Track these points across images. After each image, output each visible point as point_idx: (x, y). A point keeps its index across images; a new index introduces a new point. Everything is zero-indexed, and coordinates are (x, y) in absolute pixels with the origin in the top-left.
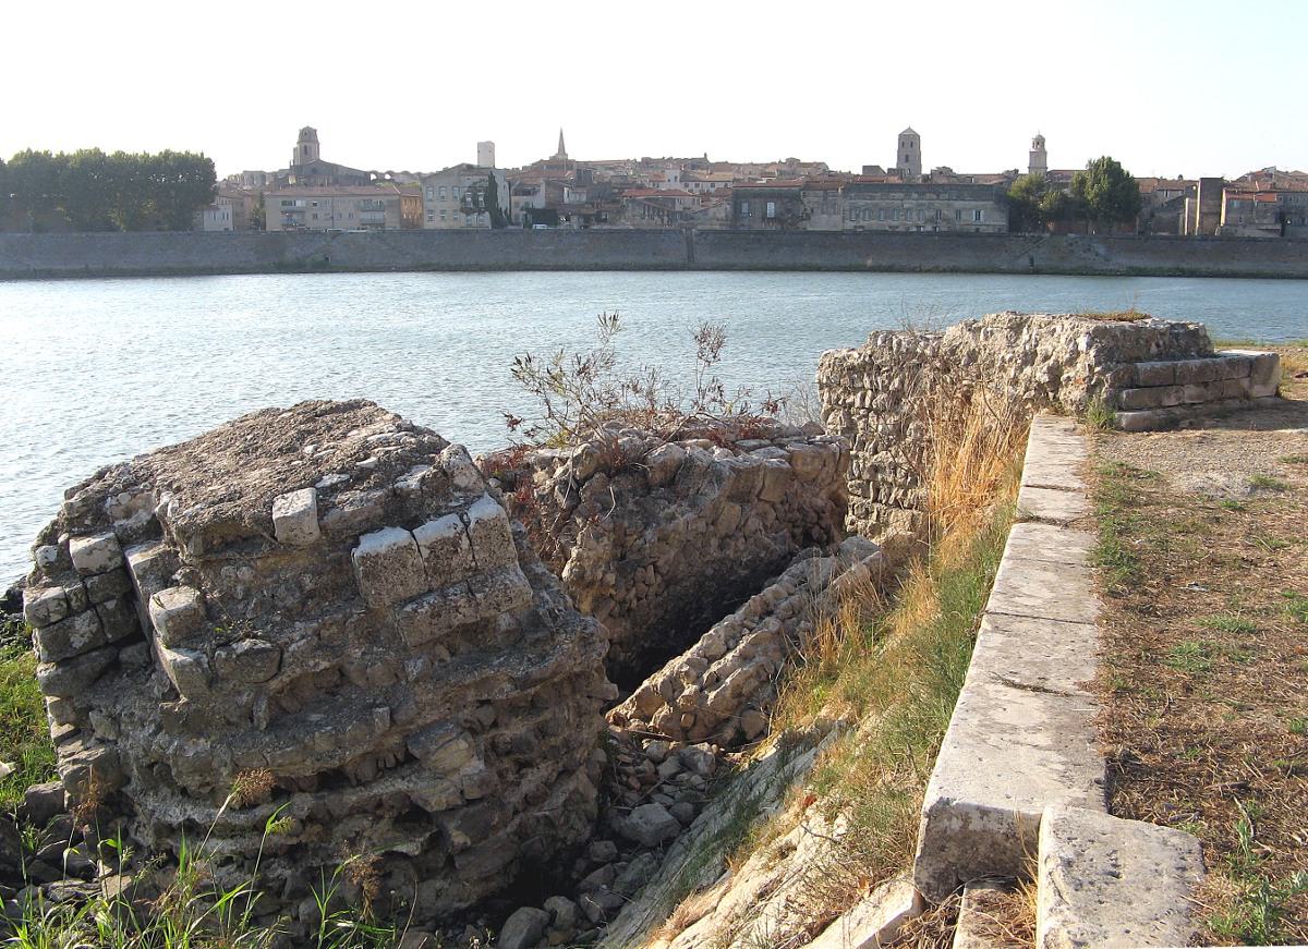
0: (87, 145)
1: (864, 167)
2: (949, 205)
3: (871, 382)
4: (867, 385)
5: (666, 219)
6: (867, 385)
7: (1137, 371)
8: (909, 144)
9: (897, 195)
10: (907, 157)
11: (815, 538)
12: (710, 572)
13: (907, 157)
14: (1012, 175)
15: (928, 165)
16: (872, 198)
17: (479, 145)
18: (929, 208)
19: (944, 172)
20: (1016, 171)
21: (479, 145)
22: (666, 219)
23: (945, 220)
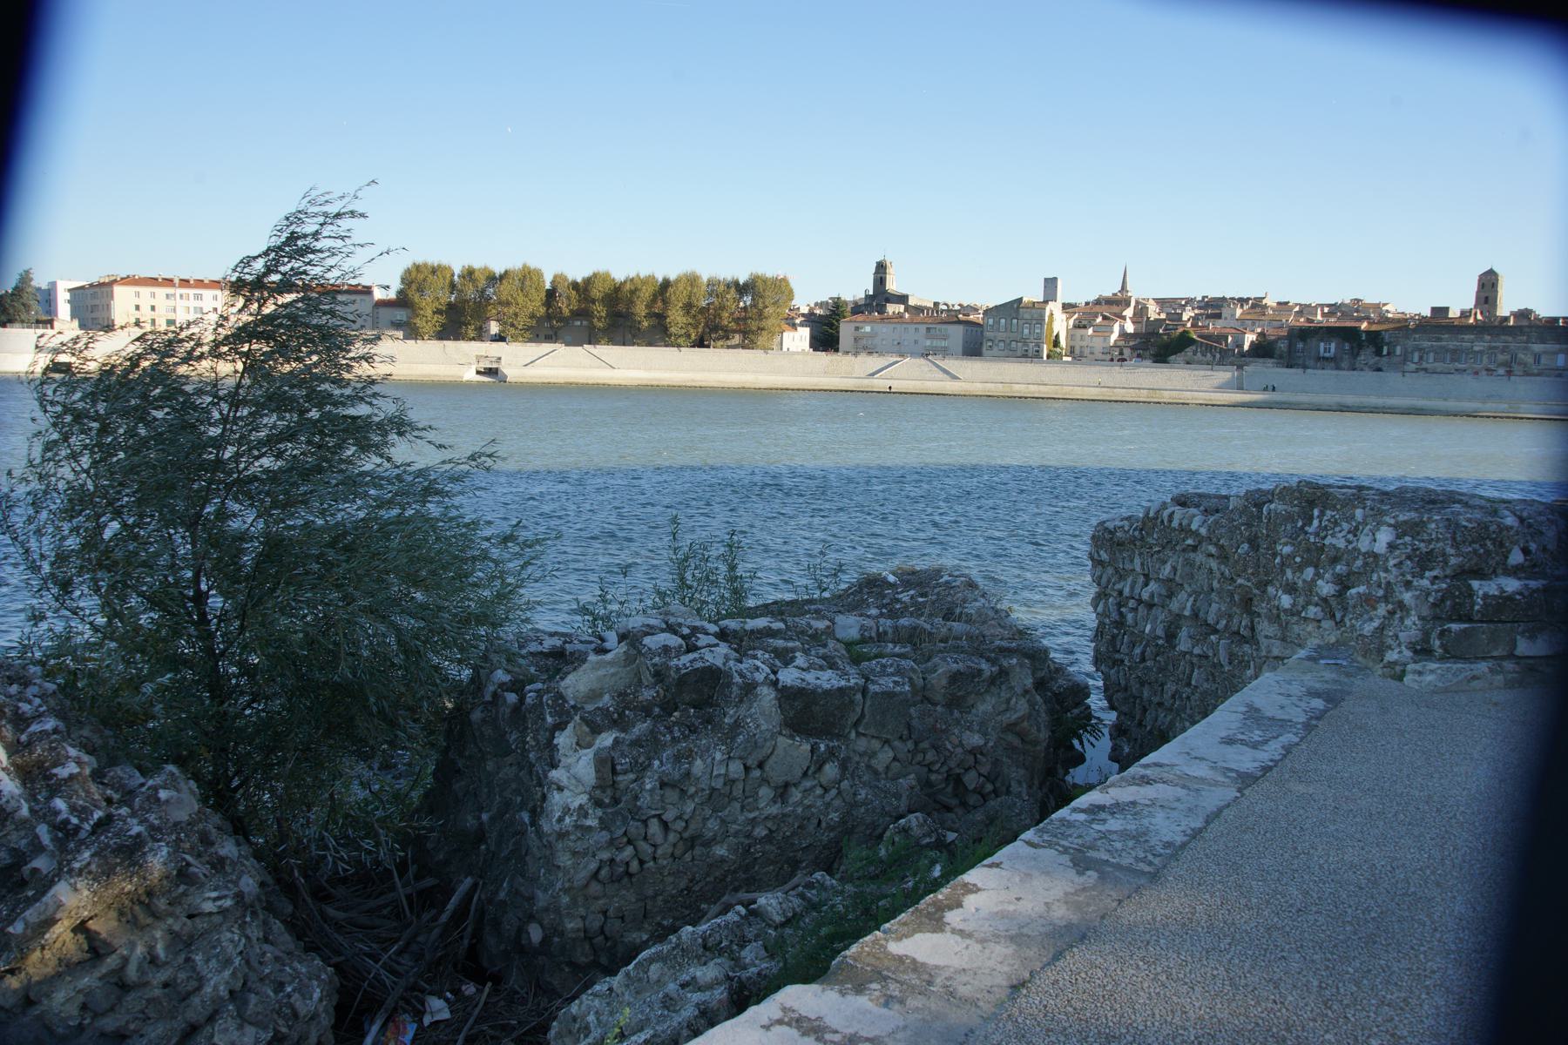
0: (1343, 296)
1: (1434, 310)
2: (1526, 348)
3: (1142, 564)
4: (1138, 569)
5: (1218, 356)
6: (1138, 569)
7: (1471, 593)
8: (1488, 285)
9: (1466, 337)
10: (1487, 298)
11: (971, 787)
12: (760, 832)
13: (1487, 298)
14: (31, 280)
15: (1506, 306)
16: (1439, 340)
17: (1046, 280)
18: (1503, 351)
19: (1524, 314)
20: (1020, 300)
21: (1046, 280)
22: (1218, 356)
23: (1520, 364)
